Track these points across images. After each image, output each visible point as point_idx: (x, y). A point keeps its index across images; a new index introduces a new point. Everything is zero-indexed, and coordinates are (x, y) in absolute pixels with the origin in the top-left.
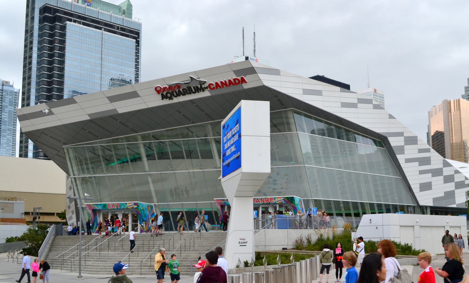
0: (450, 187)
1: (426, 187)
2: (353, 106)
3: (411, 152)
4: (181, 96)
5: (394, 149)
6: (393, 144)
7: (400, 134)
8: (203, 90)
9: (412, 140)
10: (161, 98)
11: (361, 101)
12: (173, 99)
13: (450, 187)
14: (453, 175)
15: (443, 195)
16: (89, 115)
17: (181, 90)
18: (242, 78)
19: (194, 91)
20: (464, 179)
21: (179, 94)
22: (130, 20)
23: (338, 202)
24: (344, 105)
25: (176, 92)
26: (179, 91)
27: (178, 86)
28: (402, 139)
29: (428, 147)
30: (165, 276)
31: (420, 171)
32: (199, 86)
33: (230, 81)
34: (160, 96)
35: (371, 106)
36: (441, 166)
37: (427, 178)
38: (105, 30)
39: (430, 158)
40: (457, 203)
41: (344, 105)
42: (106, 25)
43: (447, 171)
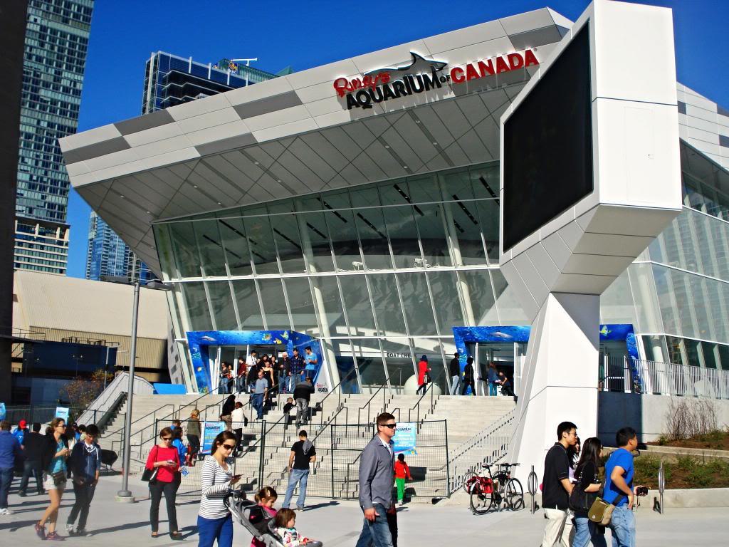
8: (437, 82)
12: (371, 107)
16: (198, 148)
18: (529, 53)
30: (448, 319)
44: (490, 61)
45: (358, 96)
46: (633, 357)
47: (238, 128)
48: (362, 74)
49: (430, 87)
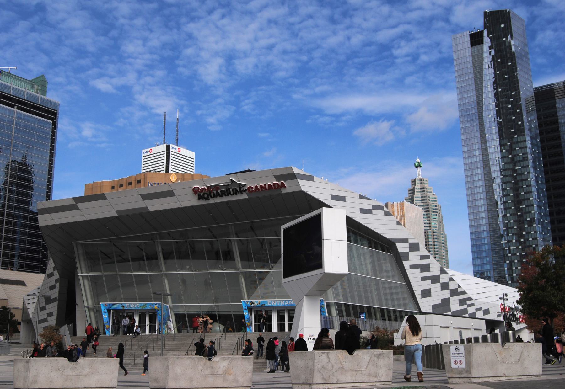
0: (446, 294)
1: (426, 293)
2: (369, 212)
3: (414, 258)
4: (218, 197)
5: (401, 255)
6: (400, 250)
7: (405, 241)
8: (241, 192)
9: (414, 247)
10: (197, 198)
11: (376, 207)
13: (446, 294)
14: (448, 283)
15: (440, 302)
16: (117, 212)
17: (219, 191)
18: (282, 183)
19: (232, 193)
20: (457, 287)
21: (217, 195)
22: (45, 97)
23: (349, 305)
24: (363, 211)
25: (213, 193)
26: (217, 192)
27: (217, 187)
28: (407, 245)
29: (427, 253)
31: (422, 278)
32: (238, 189)
33: (269, 185)
34: (196, 197)
35: (383, 212)
36: (438, 273)
37: (427, 284)
38: (18, 108)
39: (429, 265)
40: (452, 310)
41: (363, 211)
42: (19, 102)
43: (444, 279)
45: (204, 195)
47: (140, 204)
48: (206, 186)
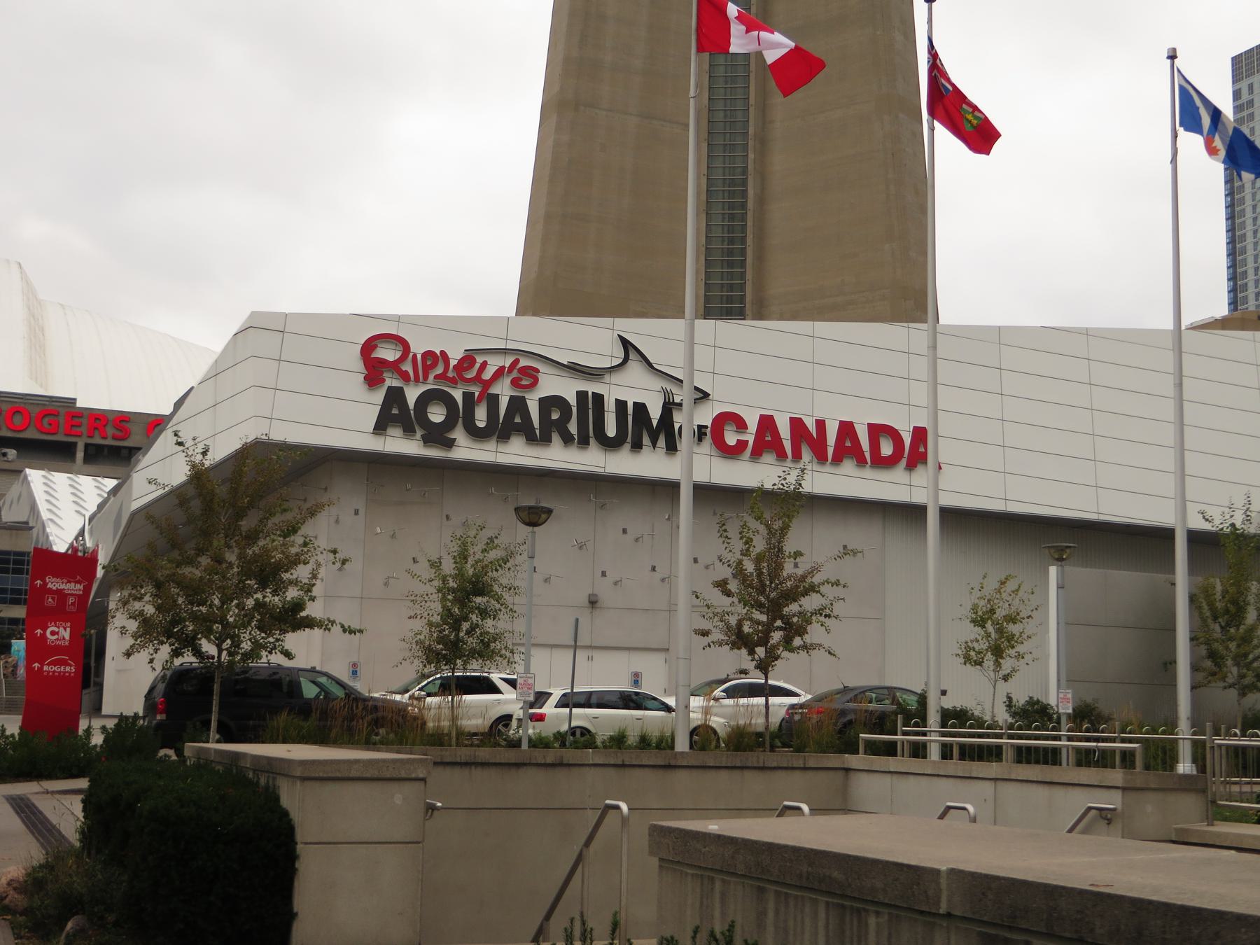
44: (821, 424)
46: (229, 641)
49: (646, 440)
